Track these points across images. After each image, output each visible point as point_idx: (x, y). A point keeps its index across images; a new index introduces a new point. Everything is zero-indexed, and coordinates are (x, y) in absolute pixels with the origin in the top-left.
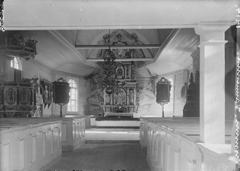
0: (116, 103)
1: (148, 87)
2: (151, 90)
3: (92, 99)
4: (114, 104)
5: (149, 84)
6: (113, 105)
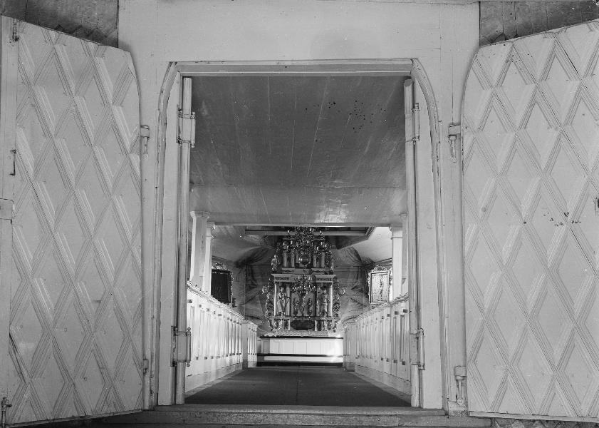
0: (296, 313)
1: (356, 284)
2: (361, 291)
3: (249, 306)
4: (293, 315)
5: (357, 278)
6: (290, 316)
